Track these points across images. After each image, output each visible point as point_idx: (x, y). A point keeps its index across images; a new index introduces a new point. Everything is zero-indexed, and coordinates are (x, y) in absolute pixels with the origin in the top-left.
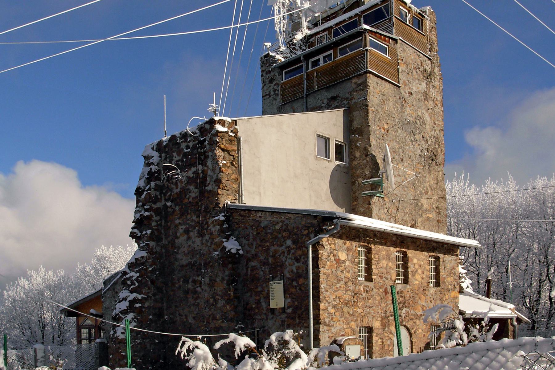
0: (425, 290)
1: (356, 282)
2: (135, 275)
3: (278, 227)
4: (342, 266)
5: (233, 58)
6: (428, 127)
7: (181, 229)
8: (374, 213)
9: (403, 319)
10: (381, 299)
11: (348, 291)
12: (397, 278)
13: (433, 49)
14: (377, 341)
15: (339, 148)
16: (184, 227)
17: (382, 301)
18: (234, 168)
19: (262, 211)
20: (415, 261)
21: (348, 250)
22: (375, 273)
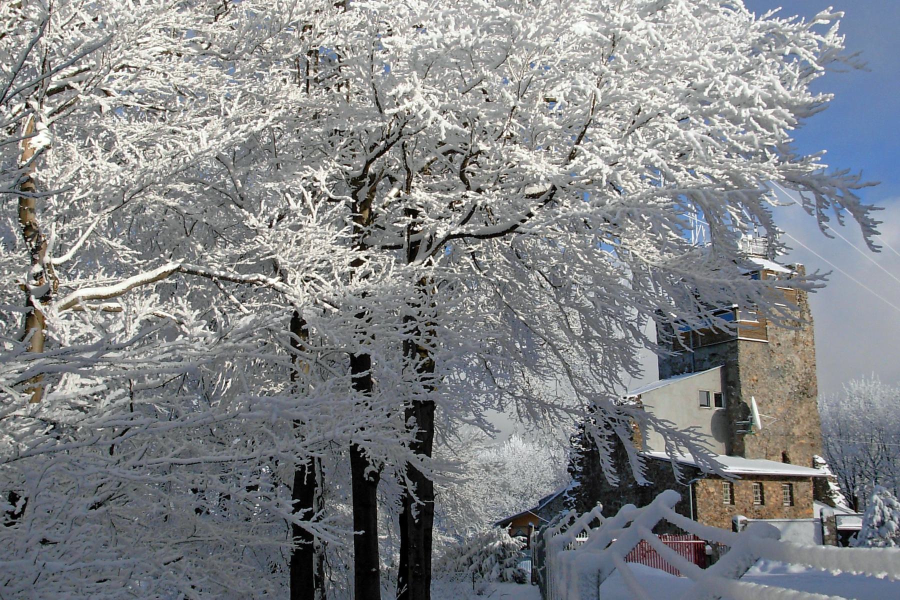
2: (573, 499)
6: (798, 367)
8: (747, 451)
15: (718, 397)
20: (770, 488)
21: (716, 485)
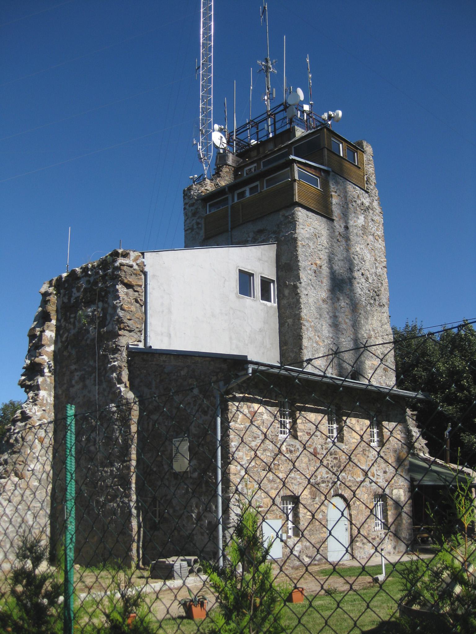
0: (365, 450)
1: (276, 440)
3: (183, 373)
4: (258, 420)
5: (230, 214)
6: (367, 264)
7: (76, 377)
9: (338, 486)
10: (309, 460)
11: (267, 451)
12: (371, 440)
13: (371, 182)
14: (305, 514)
16: (79, 373)
17: (310, 464)
18: (138, 305)
19: (167, 354)
22: (300, 429)
